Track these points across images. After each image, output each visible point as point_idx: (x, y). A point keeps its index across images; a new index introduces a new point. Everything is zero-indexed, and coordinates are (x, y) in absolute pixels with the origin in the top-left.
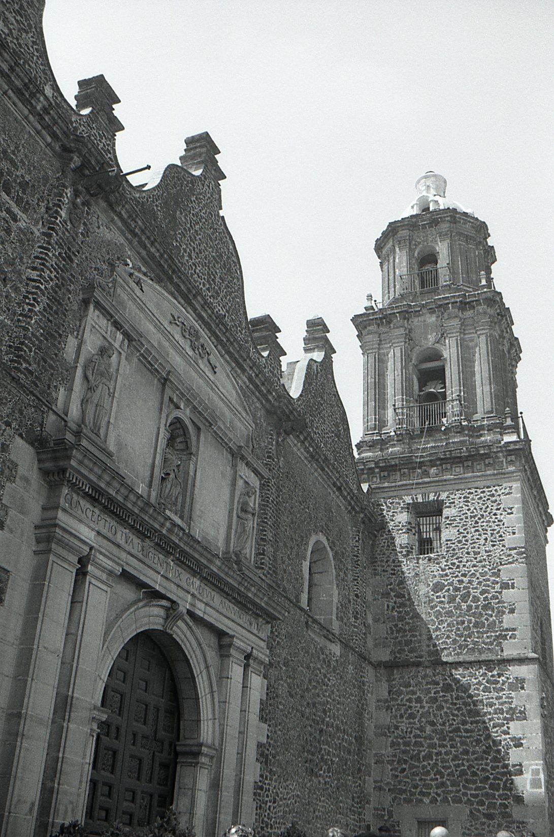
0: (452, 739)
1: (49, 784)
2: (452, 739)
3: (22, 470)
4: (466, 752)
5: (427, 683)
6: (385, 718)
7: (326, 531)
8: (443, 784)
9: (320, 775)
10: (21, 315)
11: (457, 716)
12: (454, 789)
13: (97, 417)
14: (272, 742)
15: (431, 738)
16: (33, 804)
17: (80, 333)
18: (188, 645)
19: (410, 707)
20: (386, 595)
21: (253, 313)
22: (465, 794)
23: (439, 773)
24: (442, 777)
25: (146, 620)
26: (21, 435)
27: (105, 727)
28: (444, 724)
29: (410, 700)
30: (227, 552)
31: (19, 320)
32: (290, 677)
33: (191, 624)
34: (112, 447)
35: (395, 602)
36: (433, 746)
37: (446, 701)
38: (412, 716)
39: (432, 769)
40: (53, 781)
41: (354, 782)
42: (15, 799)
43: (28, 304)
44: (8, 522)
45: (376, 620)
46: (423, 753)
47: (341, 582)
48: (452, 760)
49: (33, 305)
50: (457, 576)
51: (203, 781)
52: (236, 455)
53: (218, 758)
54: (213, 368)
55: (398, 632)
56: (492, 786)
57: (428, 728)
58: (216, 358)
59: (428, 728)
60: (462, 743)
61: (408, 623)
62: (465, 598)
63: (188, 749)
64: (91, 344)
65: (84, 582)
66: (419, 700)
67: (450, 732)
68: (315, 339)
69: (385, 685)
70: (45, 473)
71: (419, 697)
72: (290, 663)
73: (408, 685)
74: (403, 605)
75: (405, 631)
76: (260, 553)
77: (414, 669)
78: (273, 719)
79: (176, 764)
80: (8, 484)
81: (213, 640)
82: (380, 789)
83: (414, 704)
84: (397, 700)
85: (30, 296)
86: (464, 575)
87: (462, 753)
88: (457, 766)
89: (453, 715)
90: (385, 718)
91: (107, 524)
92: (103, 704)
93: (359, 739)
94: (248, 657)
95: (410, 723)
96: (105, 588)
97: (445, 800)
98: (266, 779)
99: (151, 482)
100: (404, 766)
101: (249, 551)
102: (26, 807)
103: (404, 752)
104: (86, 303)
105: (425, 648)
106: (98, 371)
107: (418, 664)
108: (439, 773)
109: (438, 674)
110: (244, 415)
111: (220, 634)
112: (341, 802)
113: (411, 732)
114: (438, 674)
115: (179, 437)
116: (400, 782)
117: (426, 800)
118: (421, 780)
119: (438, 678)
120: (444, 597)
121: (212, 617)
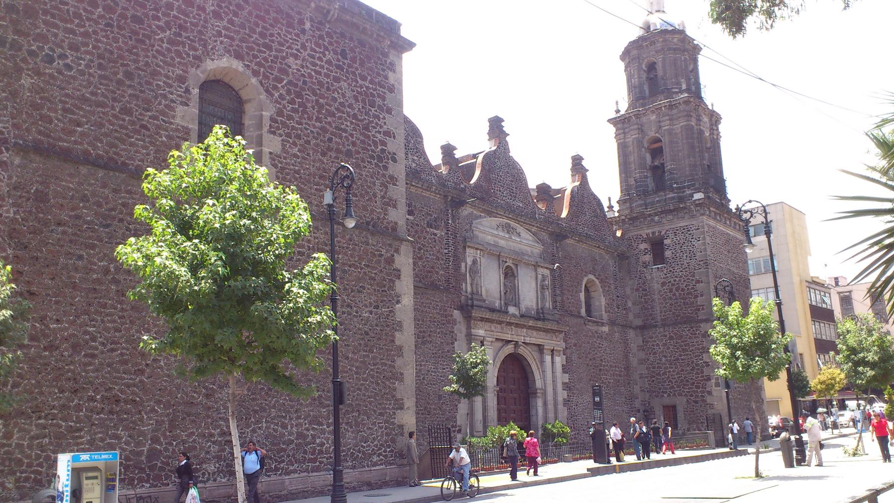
4: (682, 370)
6: (642, 355)
8: (673, 387)
13: (477, 288)
20: (637, 290)
21: (532, 183)
23: (670, 381)
27: (500, 391)
30: (538, 309)
34: (484, 297)
36: (666, 368)
38: (655, 353)
45: (633, 304)
47: (606, 293)
51: (540, 403)
52: (536, 266)
53: (544, 394)
56: (696, 387)
57: (664, 359)
58: (520, 229)
59: (664, 359)
62: (677, 290)
64: (469, 261)
66: (658, 345)
69: (641, 339)
70: (465, 318)
74: (646, 295)
76: (555, 302)
81: (536, 348)
82: (643, 391)
90: (642, 355)
93: (627, 368)
94: (552, 351)
101: (549, 304)
104: (464, 248)
106: (475, 270)
108: (670, 381)
111: (539, 345)
115: (509, 274)
117: (666, 395)
119: (667, 333)
121: (534, 341)
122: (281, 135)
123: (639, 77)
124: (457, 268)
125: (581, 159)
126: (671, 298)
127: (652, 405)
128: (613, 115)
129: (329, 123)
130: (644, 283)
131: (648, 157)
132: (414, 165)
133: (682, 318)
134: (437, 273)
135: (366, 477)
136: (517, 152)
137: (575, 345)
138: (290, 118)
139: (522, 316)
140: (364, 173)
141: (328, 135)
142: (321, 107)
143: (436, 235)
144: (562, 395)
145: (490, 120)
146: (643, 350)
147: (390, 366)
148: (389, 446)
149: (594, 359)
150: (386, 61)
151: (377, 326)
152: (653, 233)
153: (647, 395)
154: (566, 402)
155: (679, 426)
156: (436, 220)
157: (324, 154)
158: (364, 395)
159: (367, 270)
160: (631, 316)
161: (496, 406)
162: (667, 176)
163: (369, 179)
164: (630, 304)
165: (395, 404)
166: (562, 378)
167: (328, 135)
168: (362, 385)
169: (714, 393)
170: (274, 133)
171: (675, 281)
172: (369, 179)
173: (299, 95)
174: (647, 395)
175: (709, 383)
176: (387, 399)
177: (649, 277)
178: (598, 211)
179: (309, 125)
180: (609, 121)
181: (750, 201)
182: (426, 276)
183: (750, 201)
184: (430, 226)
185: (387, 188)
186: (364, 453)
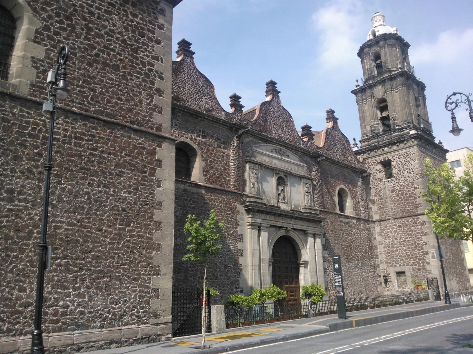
0: (403, 244)
3: (241, 212)
4: (409, 248)
8: (402, 260)
15: (396, 244)
22: (410, 263)
28: (400, 239)
29: (388, 232)
38: (389, 237)
57: (395, 241)
62: (402, 194)
66: (391, 232)
74: (381, 199)
81: (302, 233)
86: (401, 186)
88: (406, 253)
91: (263, 216)
93: (371, 248)
97: (404, 265)
102: (257, 285)
103: (389, 250)
107: (389, 219)
111: (304, 231)
119: (396, 223)
121: (299, 227)
122: (46, 45)
123: (370, 64)
125: (333, 112)
126: (398, 200)
129: (98, 43)
130: (380, 191)
131: (379, 113)
132: (207, 106)
133: (407, 213)
135: (116, 336)
136: (286, 100)
138: (56, 33)
140: (130, 84)
141: (95, 52)
142: (90, 29)
143: (224, 153)
146: (381, 235)
147: (147, 238)
148: (143, 308)
150: (157, 8)
151: (135, 204)
157: (90, 65)
158: (117, 263)
159: (128, 158)
160: (372, 213)
162: (391, 122)
163: (135, 89)
165: (150, 271)
167: (95, 52)
168: (116, 253)
169: (431, 263)
170: (39, 43)
171: (400, 188)
172: (135, 89)
173: (68, 18)
175: (427, 256)
176: (143, 267)
177: (382, 187)
178: (346, 145)
179: (77, 42)
180: (352, 92)
181: (454, 94)
183: (454, 94)
185: (152, 97)
186: (114, 314)
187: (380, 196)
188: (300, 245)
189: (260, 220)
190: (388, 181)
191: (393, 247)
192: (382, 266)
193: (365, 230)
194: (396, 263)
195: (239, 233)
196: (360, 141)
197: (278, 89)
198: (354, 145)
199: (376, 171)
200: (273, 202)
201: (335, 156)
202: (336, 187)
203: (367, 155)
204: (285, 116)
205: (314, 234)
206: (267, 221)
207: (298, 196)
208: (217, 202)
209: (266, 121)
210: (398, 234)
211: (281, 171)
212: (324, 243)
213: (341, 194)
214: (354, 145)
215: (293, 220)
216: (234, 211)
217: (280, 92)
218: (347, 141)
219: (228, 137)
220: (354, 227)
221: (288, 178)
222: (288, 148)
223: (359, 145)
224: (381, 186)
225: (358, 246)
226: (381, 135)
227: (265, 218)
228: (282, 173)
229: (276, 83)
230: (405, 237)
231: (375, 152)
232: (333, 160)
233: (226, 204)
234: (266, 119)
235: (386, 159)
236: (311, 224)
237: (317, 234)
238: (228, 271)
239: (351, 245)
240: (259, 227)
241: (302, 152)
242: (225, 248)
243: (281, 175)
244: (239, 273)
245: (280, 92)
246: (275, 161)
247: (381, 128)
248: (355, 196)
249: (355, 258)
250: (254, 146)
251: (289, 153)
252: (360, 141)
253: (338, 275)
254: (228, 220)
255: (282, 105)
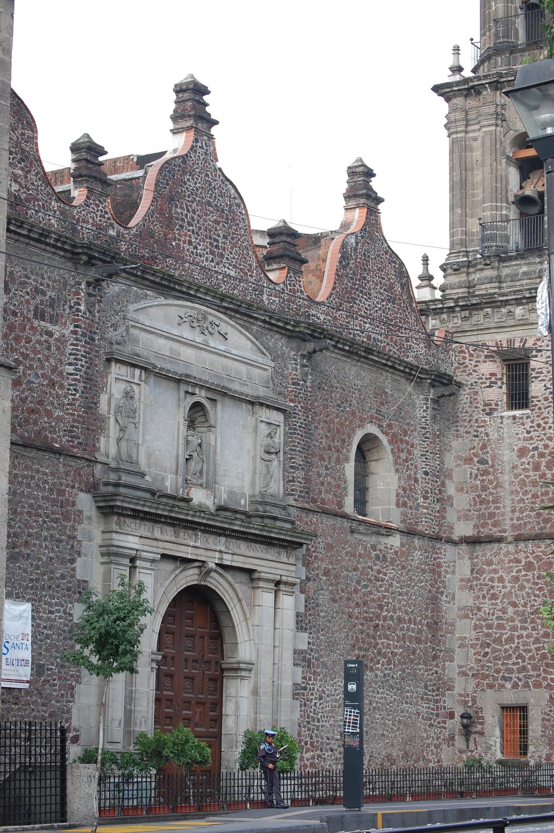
0: (533, 621)
1: (128, 707)
2: (533, 621)
3: (86, 513)
5: (510, 561)
7: (377, 420)
8: (524, 668)
9: (377, 669)
10: (68, 404)
11: (538, 596)
12: (535, 673)
14: (314, 647)
15: (513, 620)
16: (120, 720)
17: (108, 388)
18: (221, 588)
19: (493, 587)
20: (468, 461)
21: (262, 217)
22: (545, 679)
23: (520, 656)
24: (524, 661)
25: (184, 581)
26: (82, 490)
28: (525, 605)
29: (492, 580)
31: (67, 409)
32: (332, 585)
33: (221, 572)
34: (143, 467)
35: (478, 470)
37: (528, 581)
38: (494, 597)
39: (514, 652)
40: (130, 705)
41: (427, 670)
42: (110, 719)
43: (71, 394)
44: (83, 550)
45: (460, 490)
46: (505, 636)
48: (533, 643)
49: (74, 395)
50: (542, 439)
54: (224, 337)
55: (481, 503)
57: (511, 610)
60: (543, 625)
61: (491, 494)
63: (230, 666)
65: (135, 573)
66: (501, 580)
67: (532, 614)
68: (356, 196)
71: (501, 576)
72: (332, 572)
73: (489, 563)
74: (486, 472)
75: (488, 502)
77: (496, 545)
78: (314, 626)
79: (223, 677)
80: (79, 526)
81: (244, 577)
82: (464, 674)
83: (496, 584)
84: (479, 579)
85: (71, 388)
87: (543, 636)
88: (538, 649)
89: (535, 595)
91: (144, 529)
92: (159, 650)
93: (435, 626)
95: (492, 605)
96: (150, 572)
97: (526, 685)
98: (310, 679)
99: (177, 470)
100: (487, 650)
101: (277, 487)
102: (116, 723)
103: (488, 635)
105: (508, 522)
106: (128, 412)
107: (500, 540)
108: (520, 656)
109: (521, 551)
110: (260, 360)
111: (250, 572)
112: (408, 691)
113: (493, 614)
114: (521, 551)
116: (483, 666)
117: (508, 685)
118: (503, 664)
119: (521, 556)
120: (528, 464)
121: (239, 562)
124: (91, 405)
125: (369, 174)
127: (479, 704)
128: (445, 77)
130: (484, 447)
131: (514, 174)
134: (49, 414)
136: (233, 155)
137: (327, 573)
139: (221, 508)
143: (50, 334)
144: (291, 675)
145: (179, 90)
149: (365, 604)
152: (510, 341)
153: (472, 683)
154: (299, 691)
155: (531, 749)
156: (52, 303)
160: (451, 516)
161: (153, 694)
164: (451, 489)
166: (291, 639)
174: (472, 683)
177: (494, 436)
178: (398, 288)
180: (436, 89)
182: (27, 421)
184: (40, 315)
187: (483, 462)
188: (236, 614)
189: (137, 540)
190: (514, 418)
191: (500, 627)
192: (461, 686)
193: (424, 571)
194: (504, 678)
195: (79, 575)
196: (443, 268)
197: (213, 111)
198: (420, 278)
199: (483, 379)
200: (170, 483)
201: (363, 330)
202: (353, 430)
203: (458, 321)
204: (224, 202)
205: (278, 583)
206: (155, 543)
207: (241, 461)
208: (29, 486)
209: (169, 222)
210: (522, 588)
211: (202, 387)
212: (302, 610)
213: (366, 449)
214: (420, 278)
215: (223, 539)
216: (68, 513)
217: (216, 123)
218: (402, 273)
219: (65, 284)
220: (392, 562)
221: (219, 406)
222: (225, 311)
223: (439, 280)
224: (489, 430)
225: (400, 620)
226: (510, 259)
227: (149, 534)
228: (203, 393)
229: (205, 91)
230: (539, 600)
231: (486, 316)
232: (353, 343)
233: (51, 490)
234: (171, 217)
235: (517, 345)
236: (271, 553)
237: (286, 583)
238: (46, 681)
239: (378, 617)
240: (133, 560)
241: (264, 321)
242: (41, 618)
243: (201, 396)
244: (73, 688)
245: (216, 123)
246: (187, 353)
247: (514, 236)
248: (406, 460)
249: (385, 655)
250: (132, 307)
251: (227, 325)
252: (443, 268)
253: (354, 707)
254: (52, 536)
255: (219, 165)
